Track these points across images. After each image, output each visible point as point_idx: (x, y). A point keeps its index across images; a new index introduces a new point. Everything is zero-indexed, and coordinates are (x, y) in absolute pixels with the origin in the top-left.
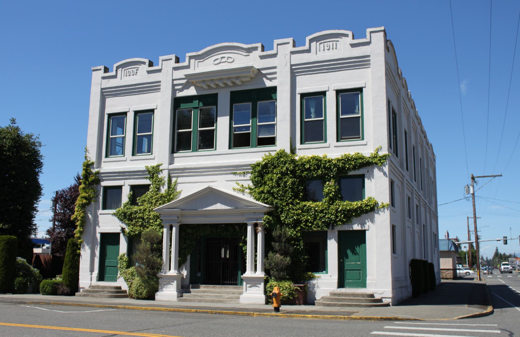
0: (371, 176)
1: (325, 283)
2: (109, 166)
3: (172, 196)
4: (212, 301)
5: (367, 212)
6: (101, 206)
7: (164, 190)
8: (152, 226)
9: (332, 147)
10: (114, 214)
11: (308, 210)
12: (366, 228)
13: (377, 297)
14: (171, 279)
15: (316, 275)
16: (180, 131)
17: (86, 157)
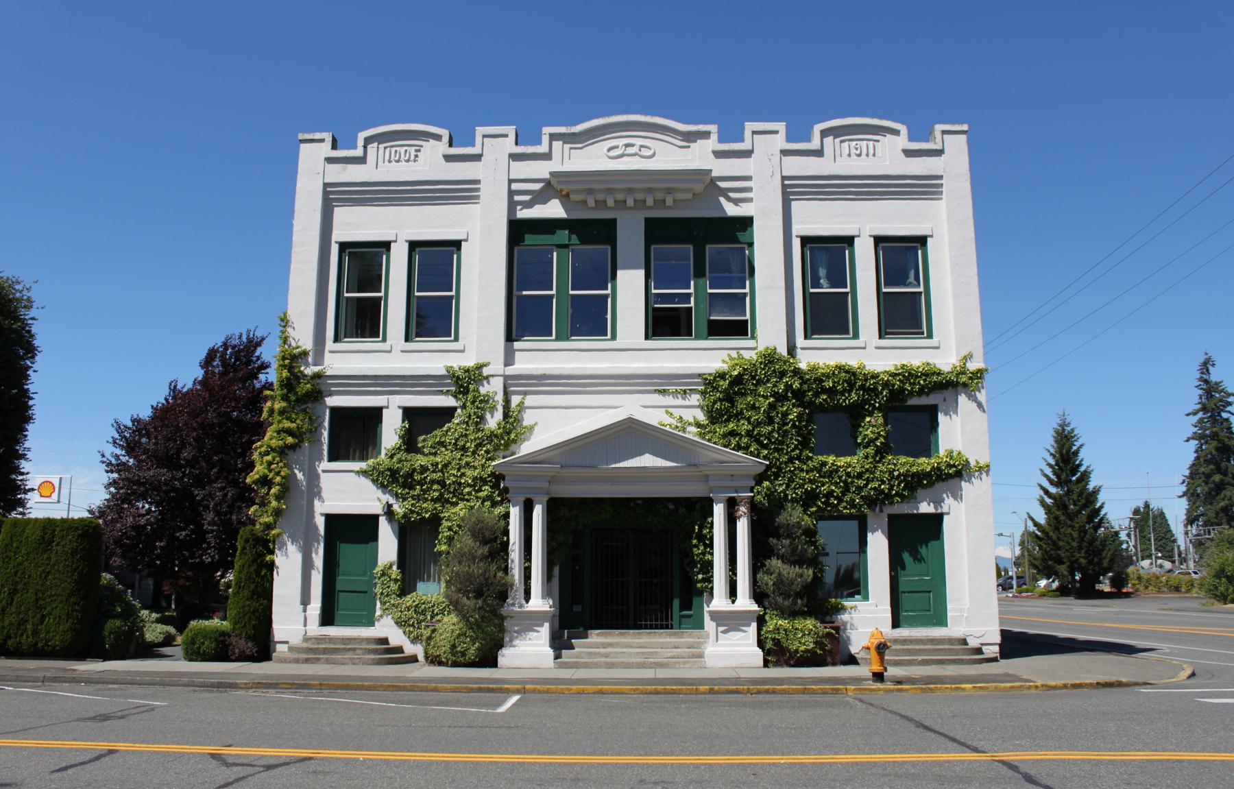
0: (953, 408)
1: (867, 619)
2: (345, 359)
3: (513, 436)
4: (641, 666)
5: (949, 476)
6: (325, 453)
7: (493, 421)
8: (468, 501)
9: (870, 349)
10: (364, 473)
11: (831, 472)
12: (945, 510)
13: (973, 643)
14: (535, 619)
15: (847, 603)
16: (524, 293)
17: (285, 340)
